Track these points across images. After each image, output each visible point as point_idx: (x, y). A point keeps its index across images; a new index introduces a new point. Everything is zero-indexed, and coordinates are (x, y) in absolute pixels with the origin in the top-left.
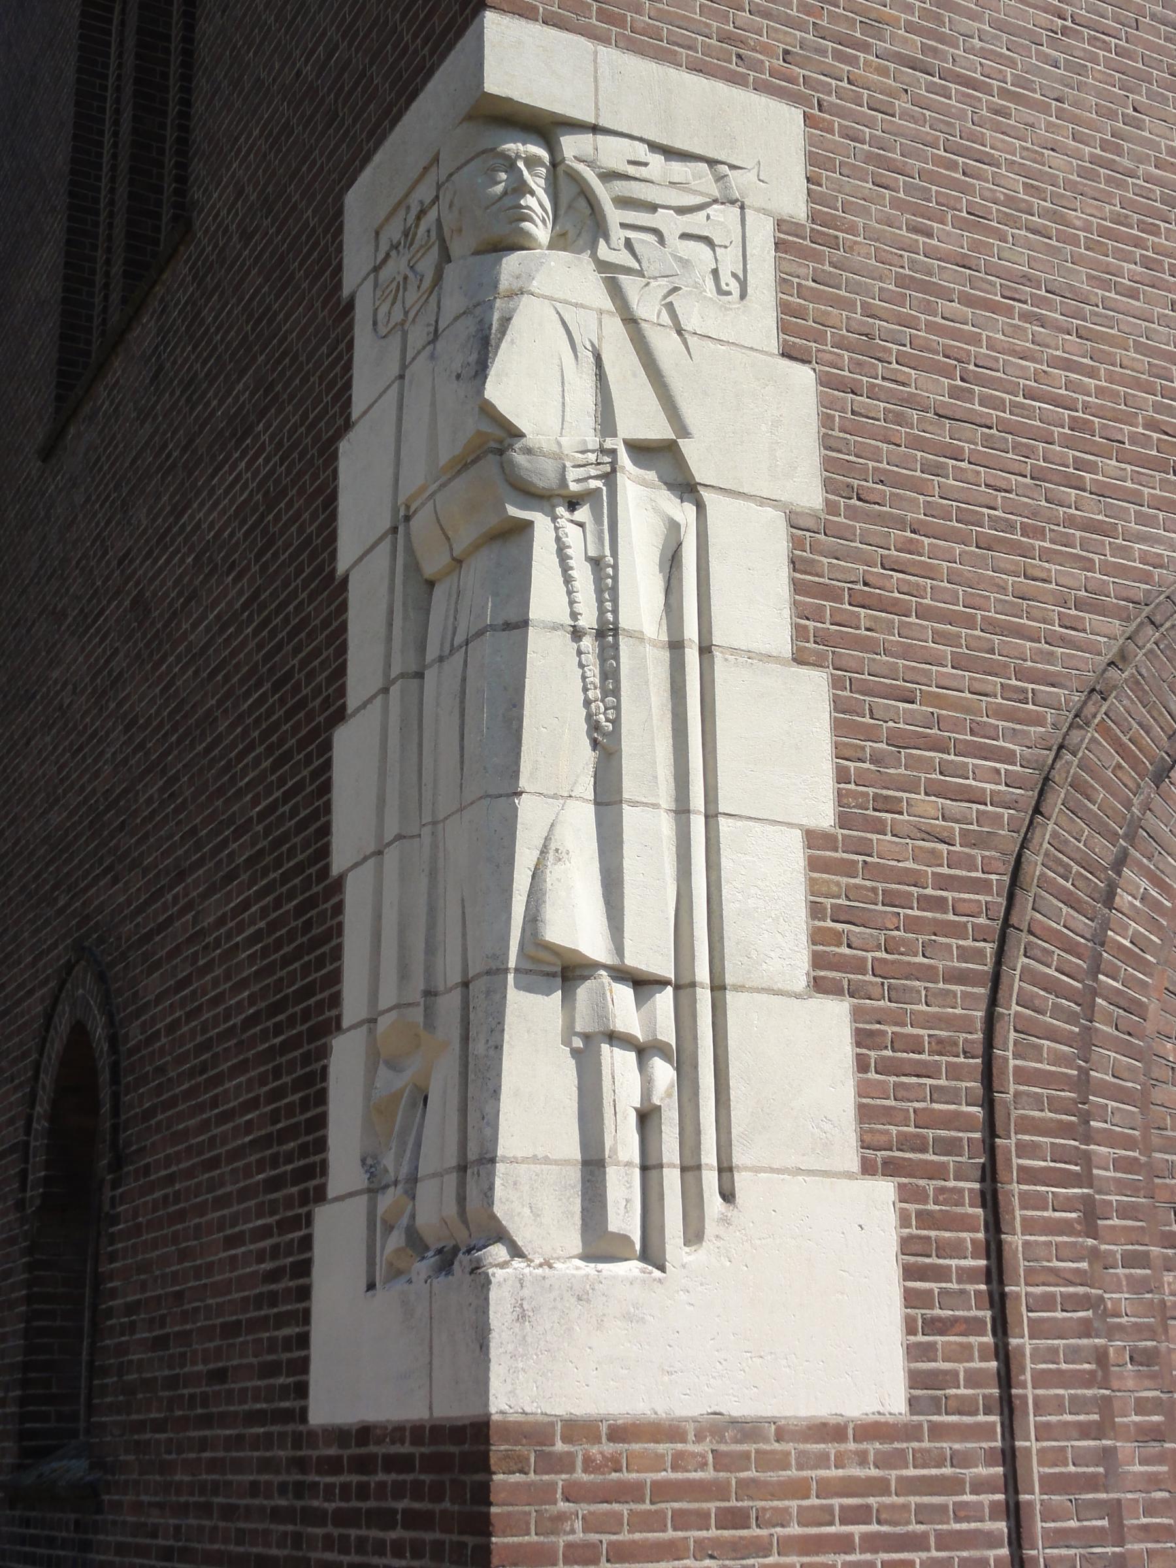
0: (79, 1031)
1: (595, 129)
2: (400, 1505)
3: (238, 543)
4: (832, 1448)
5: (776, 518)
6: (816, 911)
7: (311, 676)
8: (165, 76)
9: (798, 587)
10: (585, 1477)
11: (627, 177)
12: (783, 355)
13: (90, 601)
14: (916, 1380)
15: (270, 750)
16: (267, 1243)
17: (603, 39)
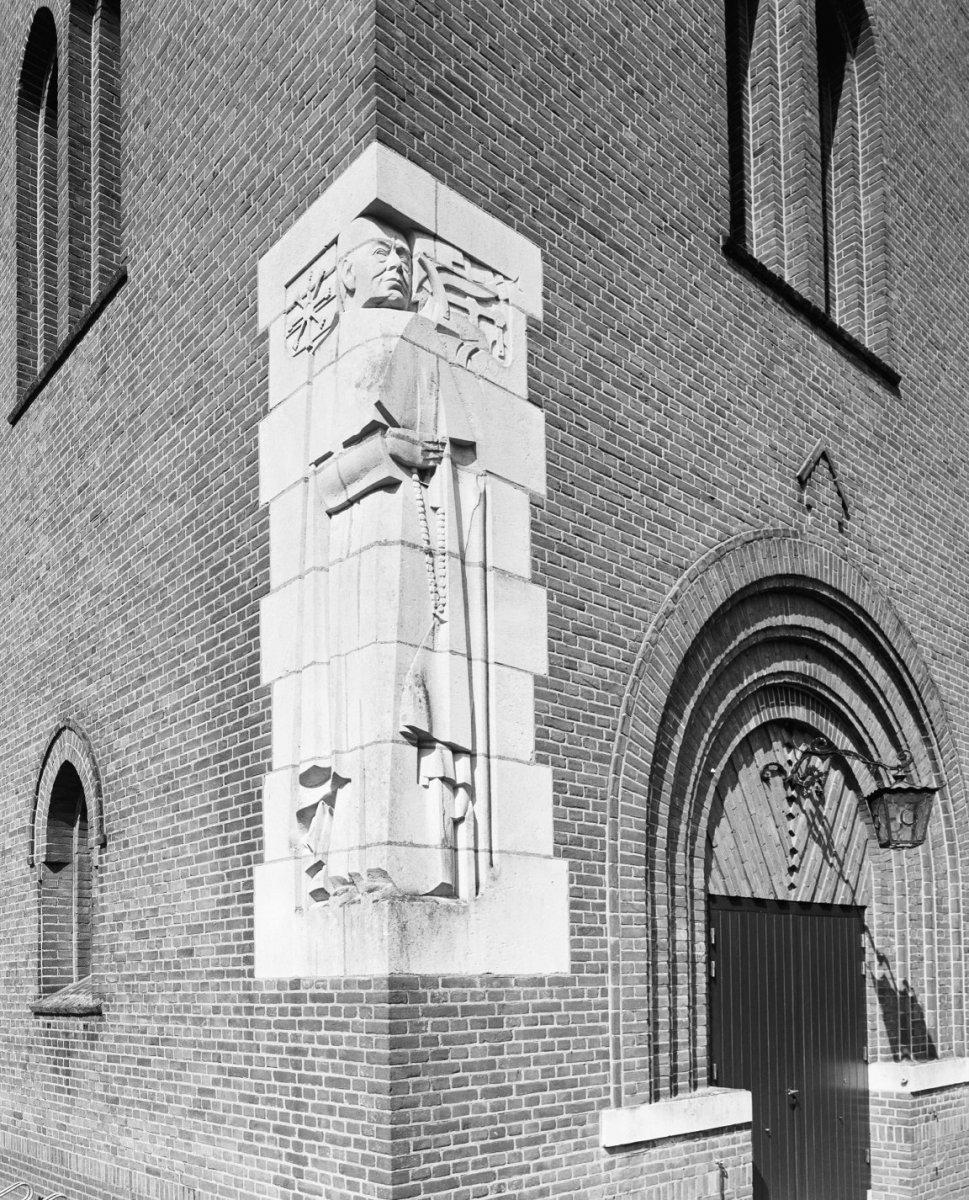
0: (67, 770)
1: (435, 237)
2: (323, 1019)
3: (177, 482)
4: (538, 989)
5: (525, 500)
6: (538, 719)
7: (240, 566)
8: (88, 170)
9: (534, 539)
10: (432, 1005)
11: (453, 273)
12: (529, 400)
13: (56, 514)
14: (575, 957)
15: (210, 609)
16: (221, 885)
17: (442, 180)
